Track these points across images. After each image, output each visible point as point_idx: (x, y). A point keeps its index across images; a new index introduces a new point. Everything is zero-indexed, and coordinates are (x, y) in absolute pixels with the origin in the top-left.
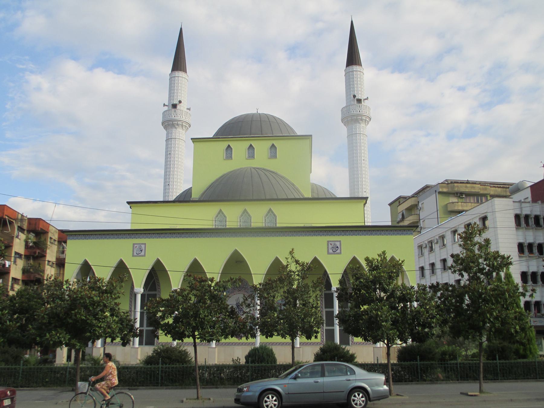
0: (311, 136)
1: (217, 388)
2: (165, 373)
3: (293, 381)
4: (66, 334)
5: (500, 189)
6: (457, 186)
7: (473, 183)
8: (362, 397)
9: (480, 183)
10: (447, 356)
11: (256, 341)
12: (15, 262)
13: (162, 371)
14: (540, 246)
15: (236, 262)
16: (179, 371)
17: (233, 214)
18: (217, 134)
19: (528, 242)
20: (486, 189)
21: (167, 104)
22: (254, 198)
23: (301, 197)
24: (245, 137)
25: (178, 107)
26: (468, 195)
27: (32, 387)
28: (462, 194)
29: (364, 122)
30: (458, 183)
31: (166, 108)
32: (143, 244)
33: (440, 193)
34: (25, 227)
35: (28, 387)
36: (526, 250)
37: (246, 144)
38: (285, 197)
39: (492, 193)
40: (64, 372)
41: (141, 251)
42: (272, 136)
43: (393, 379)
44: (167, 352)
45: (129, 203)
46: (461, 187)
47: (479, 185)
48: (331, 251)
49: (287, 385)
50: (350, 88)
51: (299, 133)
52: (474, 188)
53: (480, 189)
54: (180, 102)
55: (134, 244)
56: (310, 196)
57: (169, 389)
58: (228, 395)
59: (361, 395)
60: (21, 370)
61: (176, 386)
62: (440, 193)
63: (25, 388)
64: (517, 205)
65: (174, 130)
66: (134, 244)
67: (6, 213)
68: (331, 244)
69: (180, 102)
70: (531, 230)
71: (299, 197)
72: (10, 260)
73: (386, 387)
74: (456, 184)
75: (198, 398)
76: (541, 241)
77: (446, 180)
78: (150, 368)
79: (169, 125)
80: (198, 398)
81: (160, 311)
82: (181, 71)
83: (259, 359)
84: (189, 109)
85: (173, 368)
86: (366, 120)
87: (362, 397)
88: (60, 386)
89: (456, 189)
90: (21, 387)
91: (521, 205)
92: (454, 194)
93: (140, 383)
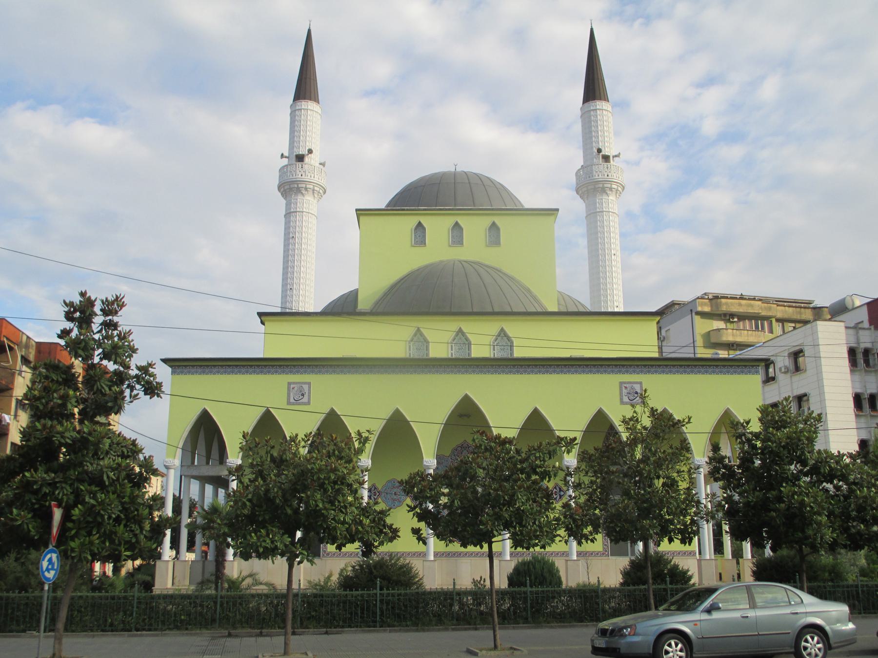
0: (557, 210)
1: (476, 629)
2: (388, 603)
3: (705, 616)
4: (283, 534)
5: (791, 309)
6: (726, 304)
7: (749, 299)
8: (818, 643)
9: (764, 300)
10: (827, 574)
11: (428, 549)
12: (16, 416)
13: (381, 601)
14: (872, 397)
15: (466, 413)
16: (410, 600)
17: (440, 336)
18: (388, 205)
19: (869, 392)
20: (770, 309)
21: (286, 154)
22: (475, 310)
23: (539, 310)
24: (446, 210)
25: (306, 159)
26: (742, 317)
27: (156, 630)
28: (732, 315)
29: (614, 193)
30: (727, 298)
31: (285, 161)
32: (305, 383)
33: (698, 313)
34: (32, 357)
35: (150, 630)
36: (866, 405)
37: (448, 221)
38: (523, 310)
39: (779, 315)
40: (212, 603)
41: (303, 395)
42: (493, 210)
43: (39, 612)
44: (381, 567)
45: (260, 315)
46: (732, 304)
47: (760, 303)
48: (626, 399)
49: (698, 623)
50: (591, 138)
51: (526, 206)
52: (752, 306)
53: (761, 308)
54: (310, 151)
55: (289, 384)
56: (556, 310)
57: (396, 631)
58: (580, 639)
59: (816, 638)
60: (136, 601)
61: (407, 626)
62: (698, 313)
63: (144, 632)
64: (851, 332)
65: (300, 197)
66: (289, 384)
67: (4, 332)
68: (626, 388)
69: (310, 151)
70: (873, 374)
71: (535, 310)
72: (9, 414)
73: (851, 626)
74: (723, 301)
75: (496, 647)
76: (874, 391)
77: (705, 294)
78: (362, 596)
79: (291, 189)
80: (496, 647)
81: (444, 494)
82: (305, 99)
83: (536, 578)
84: (323, 164)
85: (399, 595)
86: (617, 190)
87: (818, 643)
88: (207, 629)
89: (724, 308)
90: (137, 630)
91: (857, 333)
92: (720, 315)
93: (344, 621)
